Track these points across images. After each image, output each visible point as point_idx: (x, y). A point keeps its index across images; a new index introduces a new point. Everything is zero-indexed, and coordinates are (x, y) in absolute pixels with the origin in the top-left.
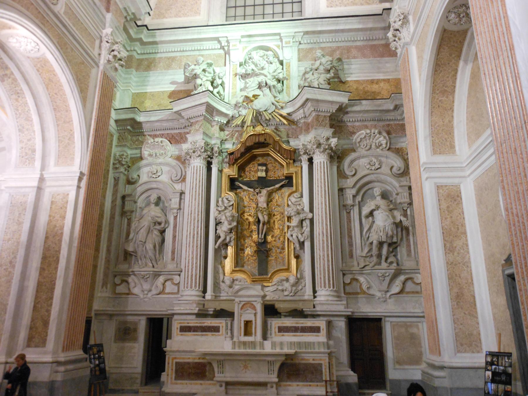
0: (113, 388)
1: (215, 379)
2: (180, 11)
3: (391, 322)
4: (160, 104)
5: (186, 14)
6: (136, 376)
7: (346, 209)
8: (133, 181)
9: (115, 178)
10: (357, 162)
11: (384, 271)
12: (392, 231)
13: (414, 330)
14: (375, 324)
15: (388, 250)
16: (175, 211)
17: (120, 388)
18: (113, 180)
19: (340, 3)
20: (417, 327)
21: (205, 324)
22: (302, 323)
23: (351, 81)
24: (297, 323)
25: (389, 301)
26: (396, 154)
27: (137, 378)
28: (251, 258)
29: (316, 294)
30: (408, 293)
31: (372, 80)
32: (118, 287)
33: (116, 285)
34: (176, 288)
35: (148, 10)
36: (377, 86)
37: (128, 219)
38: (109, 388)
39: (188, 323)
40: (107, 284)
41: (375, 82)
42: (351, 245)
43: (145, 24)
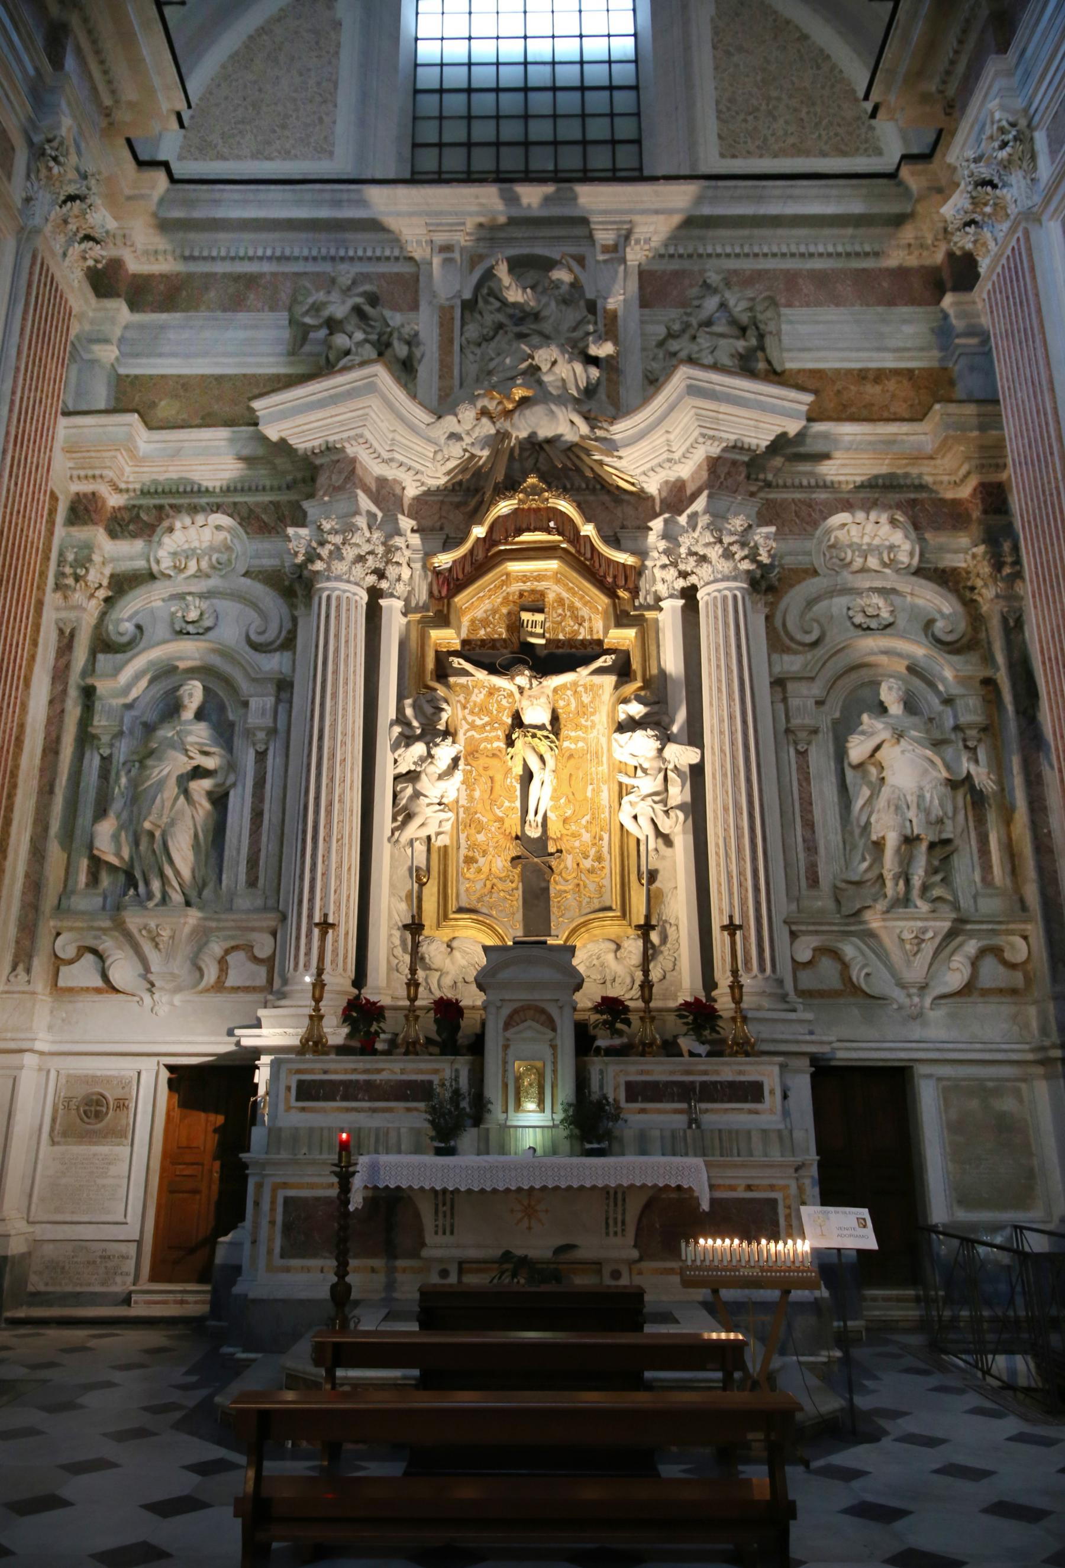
0: (42, 1288)
1: (425, 1253)
2: (269, 143)
3: (939, 1079)
4: (209, 414)
5: (288, 152)
6: (123, 1248)
7: (796, 743)
8: (124, 639)
9: (61, 631)
10: (824, 604)
11: (920, 924)
12: (941, 805)
13: (1007, 1104)
14: (893, 1082)
15: (929, 862)
16: (261, 735)
17: (69, 1289)
18: (54, 636)
19: (758, 147)
20: (1017, 1093)
21: (385, 1076)
22: (706, 1073)
23: (799, 371)
24: (688, 1073)
25: (932, 1014)
26: (940, 585)
27: (125, 1257)
28: (500, 885)
29: (713, 993)
30: (985, 993)
31: (861, 370)
32: (64, 969)
33: (58, 962)
34: (263, 971)
35: (182, 106)
36: (878, 389)
37: (103, 758)
38: (31, 1288)
39: (325, 1072)
40: (30, 957)
41: (871, 376)
42: (811, 848)
43: (162, 157)
